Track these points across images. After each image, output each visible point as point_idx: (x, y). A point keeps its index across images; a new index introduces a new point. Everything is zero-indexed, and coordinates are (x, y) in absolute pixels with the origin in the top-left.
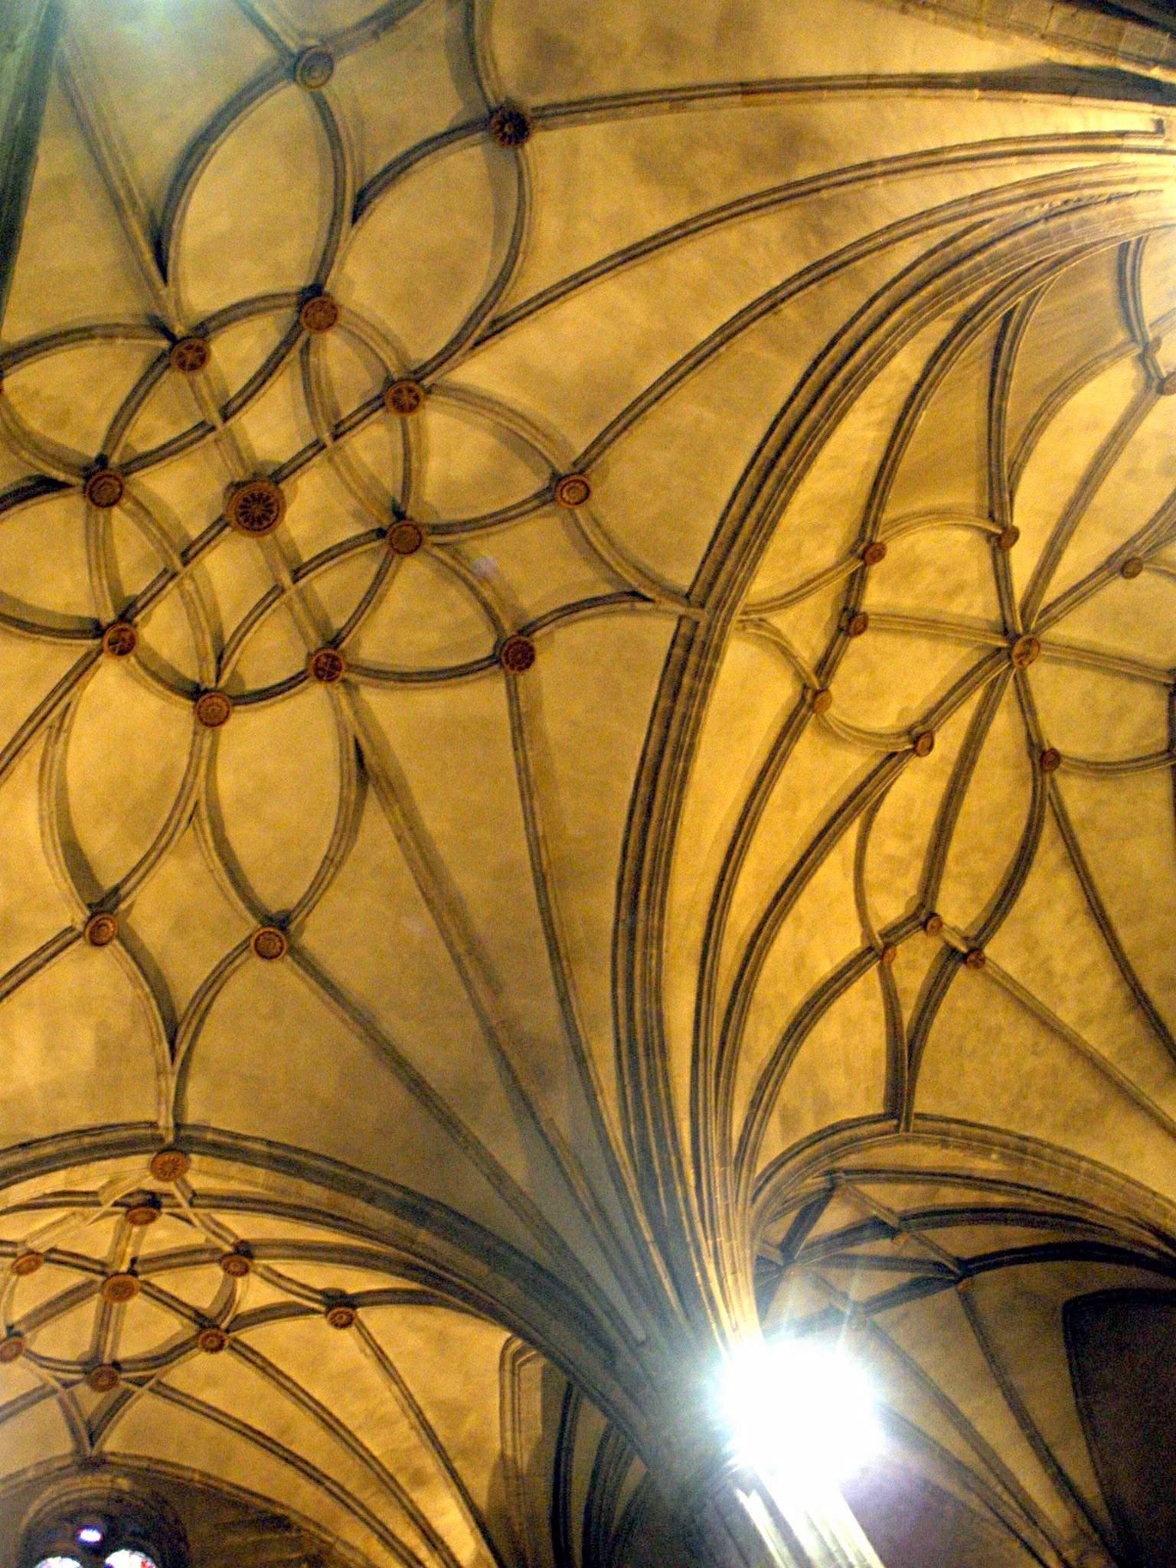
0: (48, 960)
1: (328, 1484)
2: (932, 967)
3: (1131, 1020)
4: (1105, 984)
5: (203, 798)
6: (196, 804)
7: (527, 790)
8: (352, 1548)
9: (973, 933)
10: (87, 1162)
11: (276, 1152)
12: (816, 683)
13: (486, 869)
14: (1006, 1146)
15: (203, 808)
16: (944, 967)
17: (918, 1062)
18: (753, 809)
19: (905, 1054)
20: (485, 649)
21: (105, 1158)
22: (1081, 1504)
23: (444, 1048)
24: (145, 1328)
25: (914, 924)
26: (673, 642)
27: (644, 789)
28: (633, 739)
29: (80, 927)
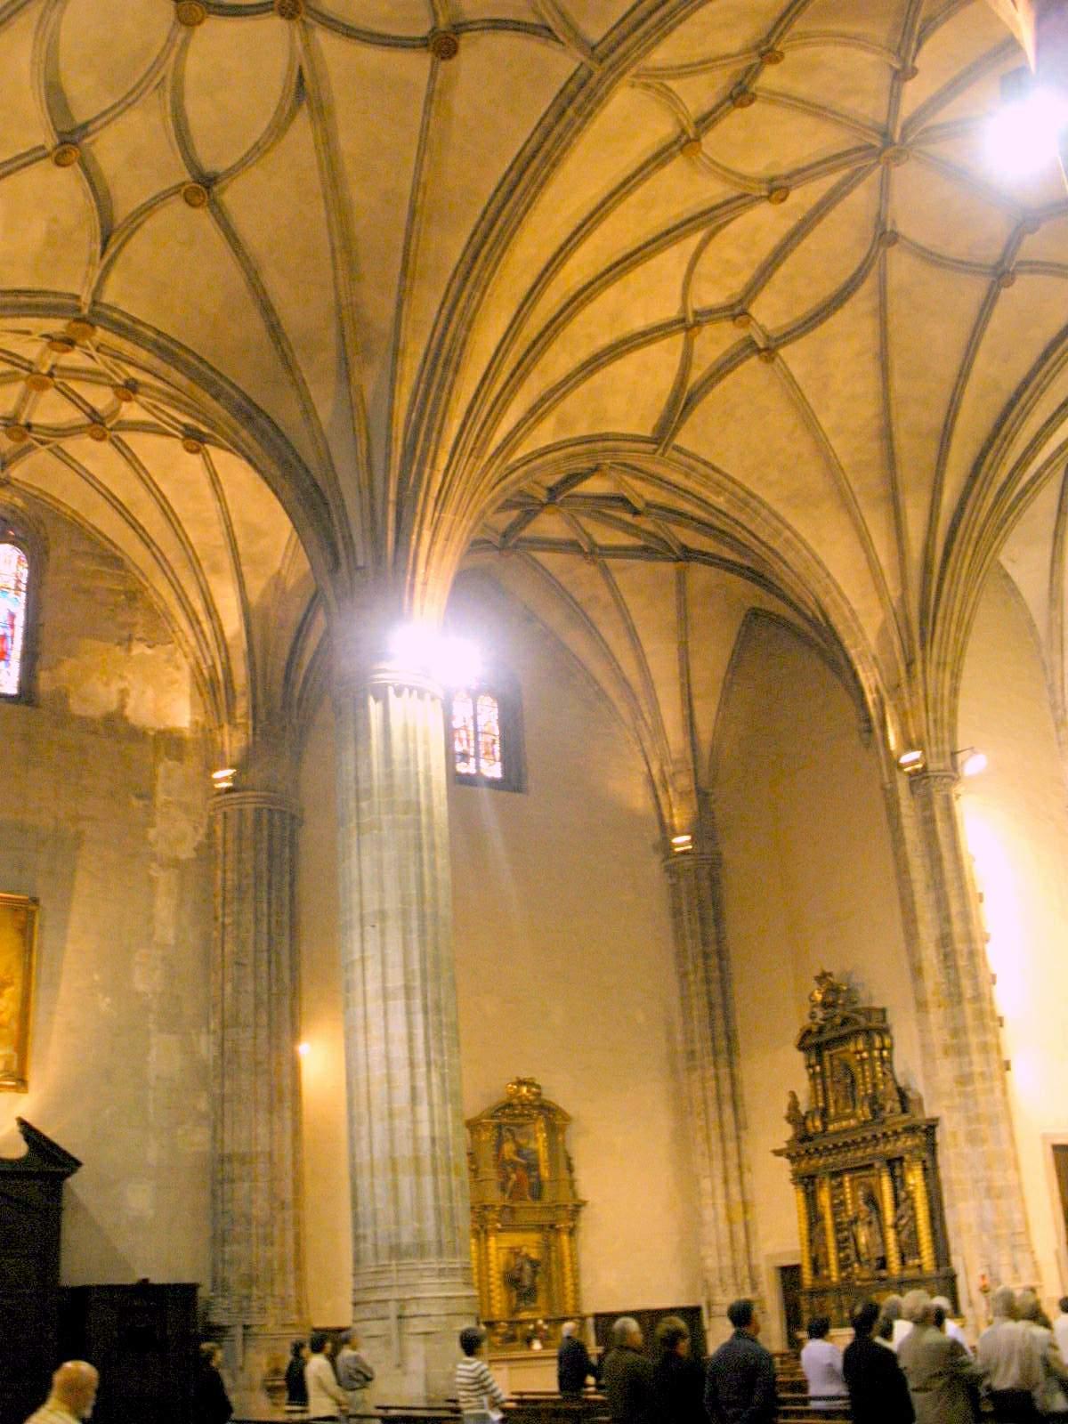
0: (18, 168)
1: (154, 549)
2: (733, 346)
3: (875, 446)
4: (868, 411)
5: (170, 77)
6: (163, 79)
7: (424, 145)
8: (159, 595)
9: (775, 335)
10: (18, 316)
11: (162, 341)
12: (691, 133)
13: (375, 195)
14: (733, 494)
15: (168, 84)
16: (742, 350)
17: (689, 413)
18: (607, 206)
19: (683, 403)
20: (423, 30)
21: (32, 316)
22: (694, 745)
23: (306, 309)
24: (51, 410)
25: (728, 313)
26: (571, 79)
27: (513, 175)
28: (517, 136)
29: (49, 147)
